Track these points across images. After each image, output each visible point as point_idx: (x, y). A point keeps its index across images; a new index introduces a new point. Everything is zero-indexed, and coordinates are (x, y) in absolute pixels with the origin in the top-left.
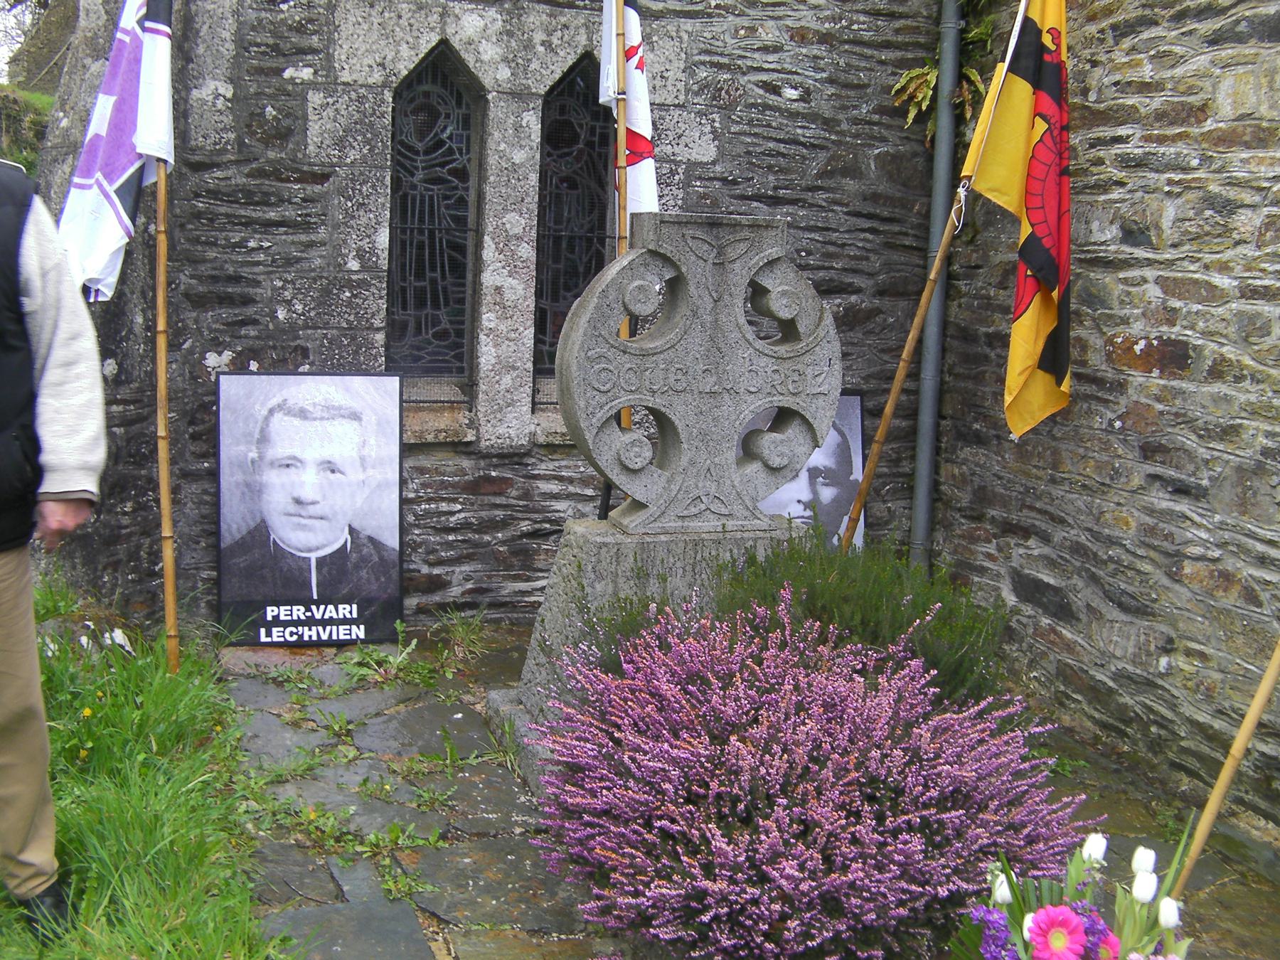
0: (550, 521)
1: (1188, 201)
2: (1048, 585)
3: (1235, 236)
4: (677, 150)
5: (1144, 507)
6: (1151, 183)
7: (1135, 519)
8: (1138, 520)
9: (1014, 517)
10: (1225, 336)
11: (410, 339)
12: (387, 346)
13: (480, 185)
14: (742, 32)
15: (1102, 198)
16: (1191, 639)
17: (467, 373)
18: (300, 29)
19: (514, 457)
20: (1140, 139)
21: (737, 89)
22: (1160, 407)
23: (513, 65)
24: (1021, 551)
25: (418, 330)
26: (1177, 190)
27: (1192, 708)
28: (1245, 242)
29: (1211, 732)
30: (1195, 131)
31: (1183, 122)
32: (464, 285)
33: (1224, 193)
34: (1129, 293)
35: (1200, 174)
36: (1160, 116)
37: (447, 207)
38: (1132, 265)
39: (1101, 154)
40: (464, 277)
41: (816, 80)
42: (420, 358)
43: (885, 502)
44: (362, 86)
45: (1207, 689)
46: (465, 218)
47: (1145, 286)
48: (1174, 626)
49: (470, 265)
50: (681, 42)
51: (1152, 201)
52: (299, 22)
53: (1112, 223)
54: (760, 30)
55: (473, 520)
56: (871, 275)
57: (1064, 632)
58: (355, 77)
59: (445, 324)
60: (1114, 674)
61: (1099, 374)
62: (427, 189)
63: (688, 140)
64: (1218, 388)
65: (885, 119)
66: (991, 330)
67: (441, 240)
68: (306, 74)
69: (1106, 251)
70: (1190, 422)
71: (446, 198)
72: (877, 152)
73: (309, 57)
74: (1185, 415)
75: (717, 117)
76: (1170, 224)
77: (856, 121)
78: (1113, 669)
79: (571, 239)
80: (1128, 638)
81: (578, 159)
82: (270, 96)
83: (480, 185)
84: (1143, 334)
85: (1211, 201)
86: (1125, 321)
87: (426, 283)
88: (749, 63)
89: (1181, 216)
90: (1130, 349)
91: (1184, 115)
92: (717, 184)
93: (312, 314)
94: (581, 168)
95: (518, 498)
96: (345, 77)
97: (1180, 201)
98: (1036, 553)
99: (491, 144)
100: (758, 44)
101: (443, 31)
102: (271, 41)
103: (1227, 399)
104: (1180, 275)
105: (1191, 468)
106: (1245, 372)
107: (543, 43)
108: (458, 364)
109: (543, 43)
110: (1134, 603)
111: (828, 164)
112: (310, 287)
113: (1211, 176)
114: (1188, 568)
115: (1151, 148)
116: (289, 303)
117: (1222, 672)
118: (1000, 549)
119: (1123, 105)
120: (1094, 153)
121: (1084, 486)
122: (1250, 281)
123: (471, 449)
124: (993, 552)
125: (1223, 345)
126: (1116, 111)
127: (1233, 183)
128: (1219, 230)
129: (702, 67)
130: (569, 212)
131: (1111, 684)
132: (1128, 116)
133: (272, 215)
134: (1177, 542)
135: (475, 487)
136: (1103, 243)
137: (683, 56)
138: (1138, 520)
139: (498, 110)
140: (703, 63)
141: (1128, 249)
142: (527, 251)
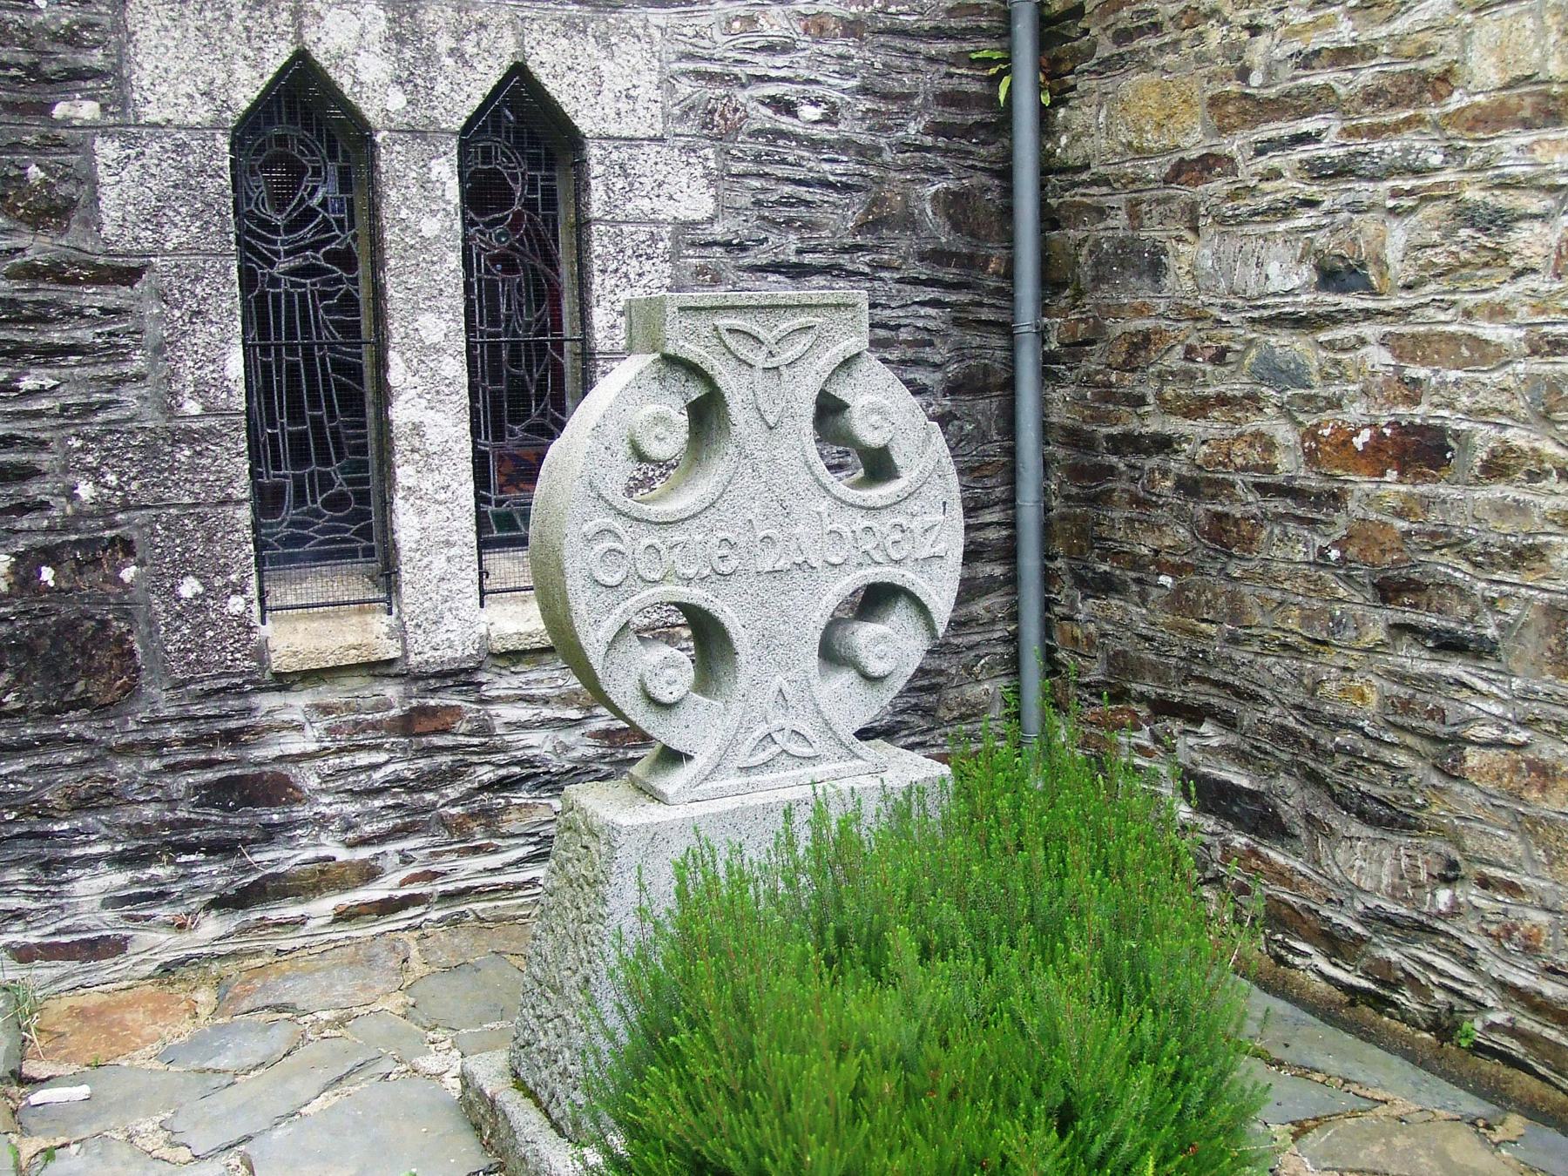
0: (520, 763)
1: (1427, 220)
2: (1239, 790)
3: (1515, 262)
4: (657, 204)
5: (1389, 672)
6: (1364, 197)
7: (1374, 692)
8: (1380, 691)
9: (1176, 694)
10: (1510, 414)
11: (289, 513)
12: (256, 527)
13: (374, 274)
14: (736, 25)
15: (1282, 227)
16: (1489, 863)
17: (378, 555)
18: (71, 38)
19: (461, 677)
20: (1340, 135)
21: (736, 110)
22: (1402, 525)
23: (409, 87)
24: (1191, 741)
25: (300, 498)
26: (1407, 202)
27: (1500, 965)
28: (1534, 271)
29: (1538, 999)
30: (1430, 112)
31: (1411, 101)
32: (363, 426)
33: (1490, 199)
34: (1337, 363)
35: (1449, 175)
36: (1372, 97)
37: (328, 310)
38: (1341, 321)
39: (1276, 162)
40: (364, 415)
41: (843, 91)
42: (307, 539)
43: (978, 681)
44: (178, 127)
45: (1527, 937)
46: (357, 324)
47: (1363, 351)
48: (1457, 842)
49: (370, 395)
50: (651, 43)
51: (1368, 225)
52: (68, 28)
53: (1300, 262)
54: (762, 21)
55: (408, 774)
56: (937, 366)
57: (1272, 854)
58: (168, 113)
59: (340, 484)
60: (1365, 915)
61: (1297, 484)
62: (294, 285)
63: (672, 190)
64: (1499, 491)
65: (942, 142)
66: (1115, 431)
67: (323, 359)
68: (88, 110)
69: (1294, 304)
70: (1459, 546)
71: (325, 296)
72: (933, 189)
73: (90, 84)
74: (1448, 535)
75: (709, 152)
76: (1400, 256)
77: (903, 147)
78: (1360, 908)
79: (514, 346)
80: (1381, 862)
81: (515, 226)
82: (33, 149)
83: (374, 274)
84: (1367, 420)
85: (1468, 215)
86: (1335, 403)
87: (307, 427)
88: (750, 71)
89: (1418, 241)
90: (1347, 443)
91: (1413, 89)
92: (718, 251)
93: (135, 485)
94: (520, 241)
95: (471, 734)
96: (152, 114)
97: (1413, 220)
98: (1214, 742)
99: (386, 213)
100: (761, 42)
101: (299, 35)
102: (25, 59)
103: (1520, 508)
104: (1422, 329)
105: (1464, 611)
106: (1548, 466)
107: (452, 52)
108: (365, 543)
109: (452, 52)
110: (1384, 811)
111: (868, 211)
112: (127, 445)
113: (1467, 177)
114: (1473, 757)
115: (1360, 144)
116: (95, 473)
117: (1549, 910)
118: (1156, 739)
119: (1310, 87)
120: (1263, 163)
121: (1285, 646)
122: (1546, 329)
123: (395, 670)
124: (1146, 743)
125: (1505, 427)
126: (1298, 97)
127: (1507, 184)
128: (1486, 256)
129: (684, 80)
130: (509, 305)
131: (1358, 929)
132: (1322, 100)
133: (56, 336)
134: (1450, 720)
135: (408, 724)
136: (1287, 293)
137: (656, 64)
138: (1380, 691)
139: (392, 159)
140: (684, 74)
141: (1331, 298)
142: (454, 368)
